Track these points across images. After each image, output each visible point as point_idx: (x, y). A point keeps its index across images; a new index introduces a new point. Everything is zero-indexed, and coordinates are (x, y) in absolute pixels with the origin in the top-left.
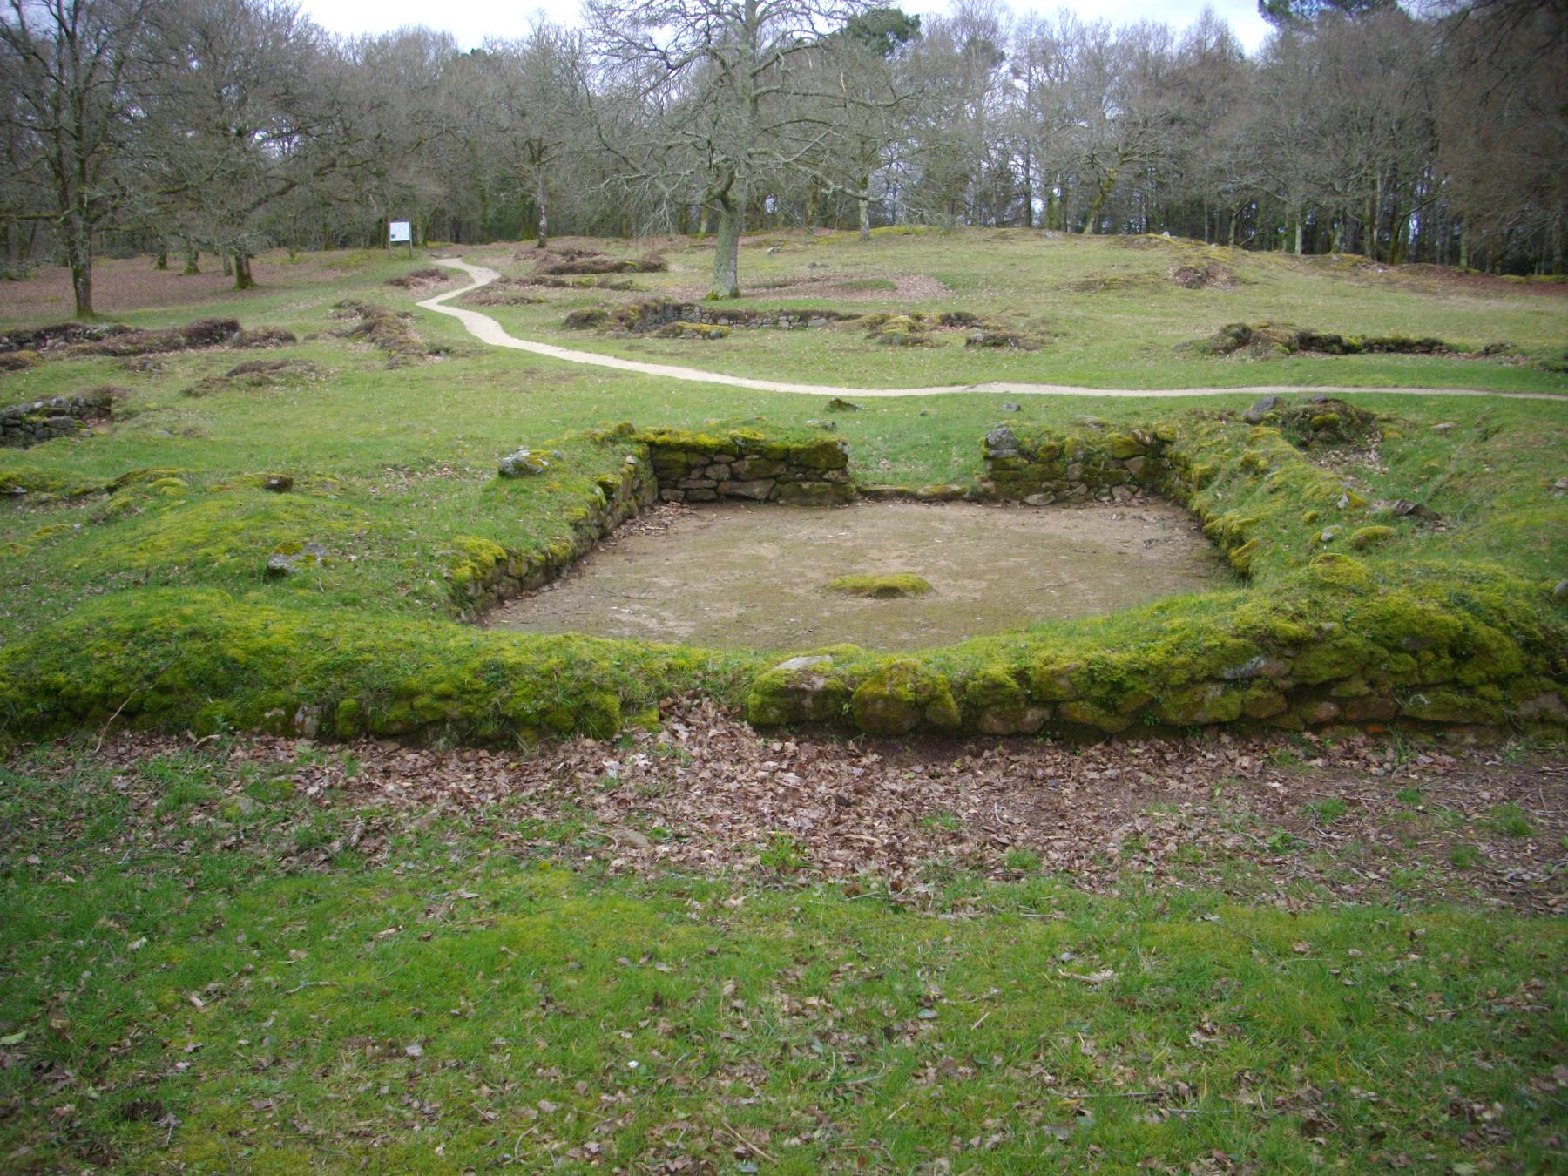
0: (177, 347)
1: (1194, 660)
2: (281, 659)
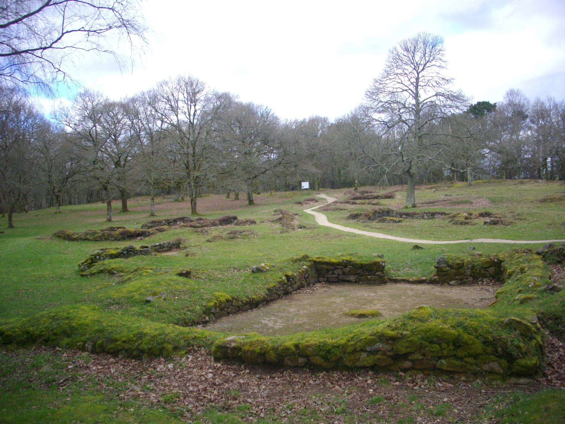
0: (216, 225)
1: (356, 343)
2: (85, 327)
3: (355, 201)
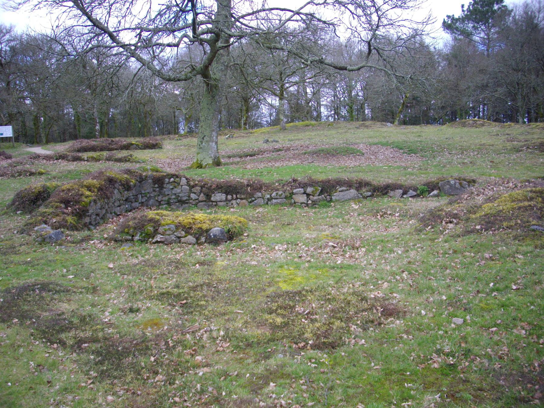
3: (80, 154)
